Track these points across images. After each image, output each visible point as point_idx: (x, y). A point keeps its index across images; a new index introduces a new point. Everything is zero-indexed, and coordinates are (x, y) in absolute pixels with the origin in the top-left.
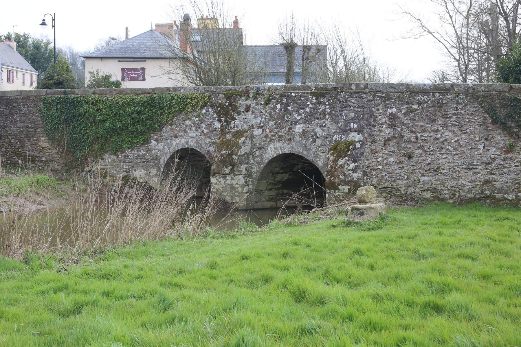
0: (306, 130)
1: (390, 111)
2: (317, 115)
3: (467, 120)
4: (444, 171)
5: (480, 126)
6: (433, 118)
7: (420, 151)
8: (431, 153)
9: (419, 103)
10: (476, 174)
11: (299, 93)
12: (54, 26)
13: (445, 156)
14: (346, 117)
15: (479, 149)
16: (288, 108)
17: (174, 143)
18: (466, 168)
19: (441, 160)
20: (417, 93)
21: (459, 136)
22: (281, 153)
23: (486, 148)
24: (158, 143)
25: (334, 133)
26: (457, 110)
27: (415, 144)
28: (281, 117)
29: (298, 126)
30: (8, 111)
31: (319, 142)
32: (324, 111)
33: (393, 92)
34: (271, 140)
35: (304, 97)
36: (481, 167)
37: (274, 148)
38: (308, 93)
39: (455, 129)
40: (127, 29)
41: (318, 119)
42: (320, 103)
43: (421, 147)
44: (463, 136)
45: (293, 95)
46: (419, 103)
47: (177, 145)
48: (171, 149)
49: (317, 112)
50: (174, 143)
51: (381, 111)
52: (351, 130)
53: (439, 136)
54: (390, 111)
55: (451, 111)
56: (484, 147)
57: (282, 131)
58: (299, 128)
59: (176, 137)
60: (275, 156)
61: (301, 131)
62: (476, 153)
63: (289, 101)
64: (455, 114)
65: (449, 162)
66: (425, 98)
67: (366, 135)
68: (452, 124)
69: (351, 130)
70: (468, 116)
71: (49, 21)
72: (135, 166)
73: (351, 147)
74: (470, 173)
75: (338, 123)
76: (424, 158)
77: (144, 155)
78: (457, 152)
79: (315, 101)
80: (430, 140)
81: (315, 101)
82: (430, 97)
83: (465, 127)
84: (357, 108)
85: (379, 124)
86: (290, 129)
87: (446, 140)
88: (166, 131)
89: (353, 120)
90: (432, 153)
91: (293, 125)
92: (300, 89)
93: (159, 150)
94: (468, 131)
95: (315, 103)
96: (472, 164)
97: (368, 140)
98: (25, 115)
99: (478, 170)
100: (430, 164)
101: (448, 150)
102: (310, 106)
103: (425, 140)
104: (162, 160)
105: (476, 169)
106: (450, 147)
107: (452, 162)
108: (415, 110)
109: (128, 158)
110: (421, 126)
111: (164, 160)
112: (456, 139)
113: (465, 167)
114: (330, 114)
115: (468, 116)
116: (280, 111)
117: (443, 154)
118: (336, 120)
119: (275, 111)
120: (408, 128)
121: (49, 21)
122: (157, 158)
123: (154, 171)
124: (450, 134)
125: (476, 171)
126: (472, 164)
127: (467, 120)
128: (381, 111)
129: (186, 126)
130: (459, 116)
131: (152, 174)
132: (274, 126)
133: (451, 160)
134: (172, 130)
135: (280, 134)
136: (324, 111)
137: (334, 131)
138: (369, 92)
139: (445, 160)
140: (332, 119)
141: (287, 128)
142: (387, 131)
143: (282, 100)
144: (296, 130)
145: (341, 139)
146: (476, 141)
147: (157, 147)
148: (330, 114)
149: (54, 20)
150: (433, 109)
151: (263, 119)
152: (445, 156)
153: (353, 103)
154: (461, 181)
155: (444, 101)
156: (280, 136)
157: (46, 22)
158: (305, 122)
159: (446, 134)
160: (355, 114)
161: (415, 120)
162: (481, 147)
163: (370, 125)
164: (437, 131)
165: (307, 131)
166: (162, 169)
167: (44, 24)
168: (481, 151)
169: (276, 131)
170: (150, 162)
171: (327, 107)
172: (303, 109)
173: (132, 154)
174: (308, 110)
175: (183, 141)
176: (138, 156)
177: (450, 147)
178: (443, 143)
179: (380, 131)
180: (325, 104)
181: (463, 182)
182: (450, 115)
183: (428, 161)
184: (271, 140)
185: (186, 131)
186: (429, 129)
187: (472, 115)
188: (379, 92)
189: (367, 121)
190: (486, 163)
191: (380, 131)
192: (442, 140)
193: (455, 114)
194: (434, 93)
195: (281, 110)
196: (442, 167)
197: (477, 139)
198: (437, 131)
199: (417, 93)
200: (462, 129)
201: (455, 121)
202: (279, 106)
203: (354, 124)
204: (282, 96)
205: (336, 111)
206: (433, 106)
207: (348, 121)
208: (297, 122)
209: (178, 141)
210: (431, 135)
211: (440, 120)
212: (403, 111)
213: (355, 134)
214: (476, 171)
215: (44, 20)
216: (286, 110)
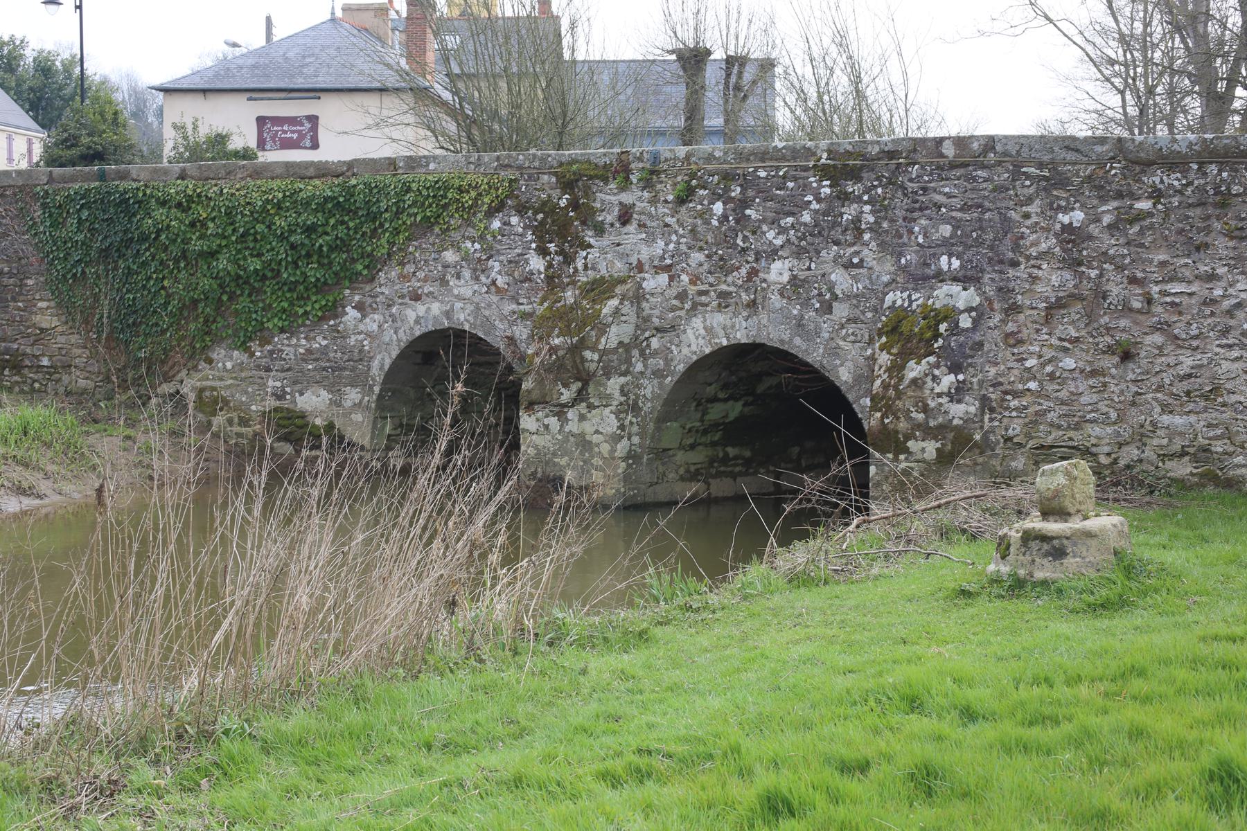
0: (802, 275)
2: (837, 233)
7: (1158, 338)
8: (1195, 344)
9: (1157, 195)
11: (778, 168)
13: (1235, 353)
14: (925, 236)
16: (748, 212)
17: (411, 315)
19: (1226, 365)
20: (1150, 164)
22: (725, 343)
24: (364, 316)
25: (887, 285)
28: (726, 240)
29: (777, 265)
31: (841, 311)
32: (857, 220)
33: (1074, 164)
34: (695, 306)
35: (795, 179)
38: (806, 169)
41: (837, 243)
42: (844, 197)
45: (762, 174)
46: (1157, 195)
49: (835, 224)
50: (411, 315)
51: (1034, 219)
53: (1218, 292)
57: (730, 279)
58: (779, 272)
59: (416, 298)
60: (707, 351)
61: (786, 278)
63: (750, 193)
66: (1175, 179)
67: (990, 290)
69: (940, 277)
72: (301, 382)
73: (943, 327)
75: (900, 255)
77: (324, 350)
79: (828, 191)
80: (1190, 306)
81: (828, 191)
82: (1192, 175)
84: (960, 210)
85: (1028, 258)
86: (753, 273)
88: (388, 281)
89: (947, 246)
90: (1195, 343)
91: (763, 263)
92: (783, 158)
95: (829, 199)
97: (996, 306)
100: (1190, 376)
102: (815, 206)
103: (1173, 304)
104: (375, 364)
108: (1141, 216)
110: (1163, 264)
111: (381, 363)
114: (875, 229)
116: (721, 223)
117: (1230, 346)
118: (891, 247)
119: (708, 223)
120: (1120, 268)
123: (353, 395)
128: (1034, 219)
129: (446, 266)
131: (348, 404)
132: (706, 266)
134: (404, 277)
135: (724, 287)
136: (857, 220)
137: (886, 278)
138: (999, 163)
139: (1236, 365)
140: (882, 246)
141: (743, 271)
142: (1055, 279)
145: (911, 302)
147: (362, 327)
148: (875, 229)
150: (1198, 211)
151: (672, 246)
152: (1235, 353)
153: (949, 196)
156: (723, 295)
158: (799, 253)
160: (955, 228)
161: (1142, 245)
163: (1001, 262)
164: (1212, 277)
165: (805, 281)
166: (377, 389)
169: (711, 279)
171: (867, 208)
172: (792, 214)
173: (292, 347)
174: (806, 217)
175: (436, 308)
176: (309, 351)
178: (1230, 313)
179: (1034, 279)
180: (859, 199)
183: (1184, 369)
184: (695, 306)
186: (1187, 273)
188: (1028, 162)
189: (991, 248)
191: (1034, 279)
192: (1226, 304)
194: (1201, 165)
195: (724, 218)
196: (1228, 386)
198: (1212, 277)
199: (1150, 164)
202: (718, 208)
203: (950, 256)
204: (727, 177)
205: (892, 221)
206: (1201, 204)
207: (930, 250)
208: (773, 254)
209: (421, 309)
212: (1107, 220)
213: (956, 288)
216: (742, 220)
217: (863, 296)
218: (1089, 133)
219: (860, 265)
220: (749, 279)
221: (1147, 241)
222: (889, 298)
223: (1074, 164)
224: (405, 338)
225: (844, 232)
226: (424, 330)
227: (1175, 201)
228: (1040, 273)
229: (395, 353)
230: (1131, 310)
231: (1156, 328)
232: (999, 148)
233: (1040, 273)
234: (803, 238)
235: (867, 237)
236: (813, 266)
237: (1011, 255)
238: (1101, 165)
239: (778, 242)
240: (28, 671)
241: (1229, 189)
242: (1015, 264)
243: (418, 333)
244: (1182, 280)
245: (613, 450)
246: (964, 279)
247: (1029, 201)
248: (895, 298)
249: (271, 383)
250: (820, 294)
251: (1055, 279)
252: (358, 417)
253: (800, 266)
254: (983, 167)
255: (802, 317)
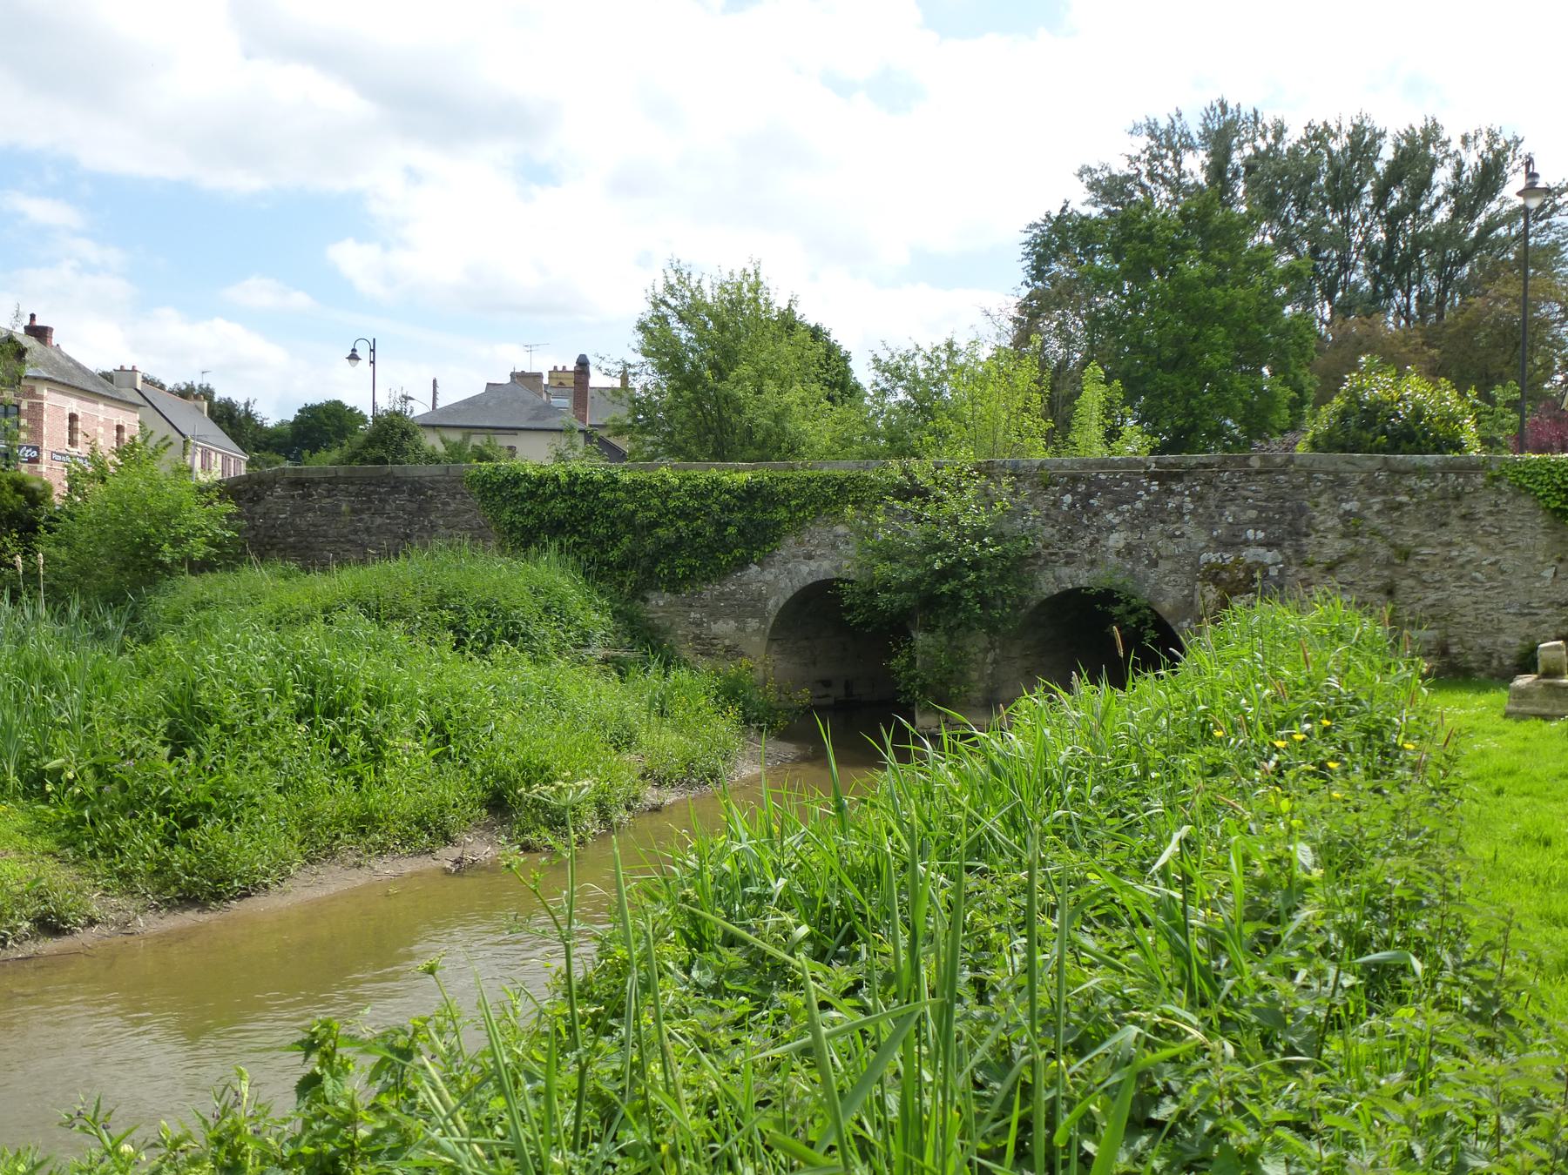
0: (1135, 543)
1: (1347, 506)
2: (1164, 516)
3: (1519, 524)
4: (1465, 619)
5: (1545, 534)
6: (1444, 519)
7: (1411, 582)
8: (1440, 585)
9: (1412, 492)
10: (1536, 624)
11: (1116, 474)
12: (373, 362)
13: (1466, 591)
14: (1234, 517)
15: (1545, 578)
16: (1092, 501)
17: (805, 569)
18: (1514, 614)
19: (1459, 599)
20: (1407, 472)
21: (1500, 553)
22: (1070, 586)
23: (1559, 575)
24: (763, 570)
25: (1202, 549)
26: (1496, 505)
27: (1400, 569)
28: (1073, 519)
29: (1115, 536)
30: (415, 506)
31: (1165, 566)
32: (1179, 508)
33: (1351, 472)
34: (1046, 563)
35: (1129, 480)
36: (1549, 611)
37: (1055, 577)
38: (1139, 474)
39: (1491, 540)
40: (435, 381)
41: (1161, 522)
42: (1170, 492)
43: (1415, 575)
44: (1509, 553)
45: (1103, 477)
46: (1412, 492)
47: (810, 573)
48: (795, 582)
49: (1162, 510)
50: (805, 569)
51: (1323, 507)
52: (1247, 543)
53: (1455, 553)
54: (1347, 506)
55: (1482, 508)
56: (1555, 574)
57: (1076, 545)
58: (1117, 540)
59: (809, 557)
60: (1056, 592)
61: (1122, 544)
62: (1537, 585)
63: (1093, 489)
64: (1491, 513)
65: (1476, 603)
66: (1426, 483)
67: (1289, 552)
68: (1486, 532)
69: (1247, 543)
70: (1519, 517)
71: (363, 352)
72: (715, 615)
73: (1258, 575)
74: (1525, 622)
75: (1212, 530)
76: (1420, 595)
77: (733, 593)
78: (1495, 584)
79: (1157, 488)
80: (1435, 562)
81: (1157, 488)
82: (1437, 481)
83: (1512, 538)
84: (1265, 501)
85: (1317, 531)
86: (1095, 541)
87: (1469, 562)
88: (788, 546)
89: (1255, 523)
90: (1438, 585)
91: (1105, 534)
92: (1119, 467)
93: (766, 583)
94: (1520, 544)
95: (1158, 493)
96: (1528, 605)
97: (1293, 562)
98: (456, 513)
99: (1542, 617)
100: (1434, 605)
101: (1474, 579)
102: (1146, 497)
103: (1423, 561)
104: (771, 602)
105: (1536, 614)
106: (1478, 575)
107: (1482, 603)
108: (1401, 504)
109: (700, 598)
110: (1416, 536)
111: (774, 604)
112: (1493, 559)
113: (1512, 611)
114: (1192, 513)
115: (1519, 517)
116: (1070, 509)
117: (1462, 587)
118: (1209, 523)
119: (1059, 508)
120: (1385, 538)
121: (363, 352)
122: (761, 598)
123: (753, 623)
124: (1479, 550)
125: (1536, 618)
126: (1528, 605)
127: (1519, 524)
128: (1323, 507)
129: (837, 536)
130: (1501, 516)
131: (749, 630)
132: (1057, 537)
133: (1481, 599)
134: (801, 544)
135: (1071, 550)
136: (1179, 508)
137: (1202, 544)
138: (1296, 471)
139: (1467, 598)
140: (1199, 524)
141: (1087, 540)
142: (1337, 545)
143: (1088, 487)
144: (1111, 543)
145: (1224, 560)
146: (1539, 562)
147: (761, 578)
148: (1192, 513)
149: (373, 350)
150: (1441, 502)
151: (1029, 524)
152: (1466, 591)
153: (1255, 492)
154: (1503, 638)
155: (1468, 489)
156: (1069, 555)
157: (358, 354)
158: (1132, 528)
159: (1469, 549)
160: (1260, 512)
161: (1401, 524)
162: (1549, 573)
163: (1298, 534)
164: (1450, 544)
165: (1138, 546)
166: (771, 620)
167: (353, 357)
168: (1548, 582)
169: (1061, 545)
170: (746, 606)
171: (1188, 499)
172: (1128, 503)
173: (710, 591)
174: (1139, 505)
175: (826, 564)
176: (722, 593)
177: (1478, 575)
178: (1462, 566)
179: (1321, 545)
180: (1181, 494)
181: (1508, 639)
182: (1481, 515)
183: (1428, 602)
184: (1046, 563)
185: (834, 546)
186: (1432, 541)
187: (1529, 514)
188: (1316, 472)
189: (1290, 525)
190: (1559, 603)
191: (1321, 545)
192: (1460, 561)
193: (1491, 513)
194: (1444, 474)
195: (1073, 505)
196: (1462, 611)
197: (1541, 559)
198: (1450, 544)
199: (1407, 472)
200: (1507, 540)
201: (1491, 525)
202: (1068, 498)
203: (1256, 530)
204: (1075, 479)
205: (1206, 508)
206: (1443, 498)
207: (1237, 527)
208: (1112, 528)
209: (813, 565)
210: (1437, 551)
211: (1456, 524)
212: (1376, 508)
213: (1262, 551)
214: (1536, 618)
215: (354, 350)
216: (1086, 507)
217: (1182, 555)
218: (585, 464)
219: (1182, 535)
220: (1092, 544)
221: (1405, 520)
222: (1204, 557)
223: (1351, 472)
224: (798, 584)
225: (1168, 515)
226: (815, 579)
227: (1425, 496)
228: (1326, 541)
229: (789, 594)
230: (1393, 564)
231: (1410, 576)
232: (1298, 461)
233: (1326, 541)
234: (1137, 518)
235: (1187, 518)
236: (1144, 537)
237: (1304, 529)
238: (1371, 473)
239: (1116, 521)
240: (1113, 640)
241: (1463, 489)
242: (1307, 535)
243: (810, 582)
244: (1429, 546)
245: (984, 659)
246: (1268, 544)
247: (1320, 494)
248: (1213, 557)
249: (692, 615)
250: (1149, 555)
251: (1337, 545)
252: (756, 639)
253: (1133, 537)
254: (1284, 473)
255: (1134, 570)
